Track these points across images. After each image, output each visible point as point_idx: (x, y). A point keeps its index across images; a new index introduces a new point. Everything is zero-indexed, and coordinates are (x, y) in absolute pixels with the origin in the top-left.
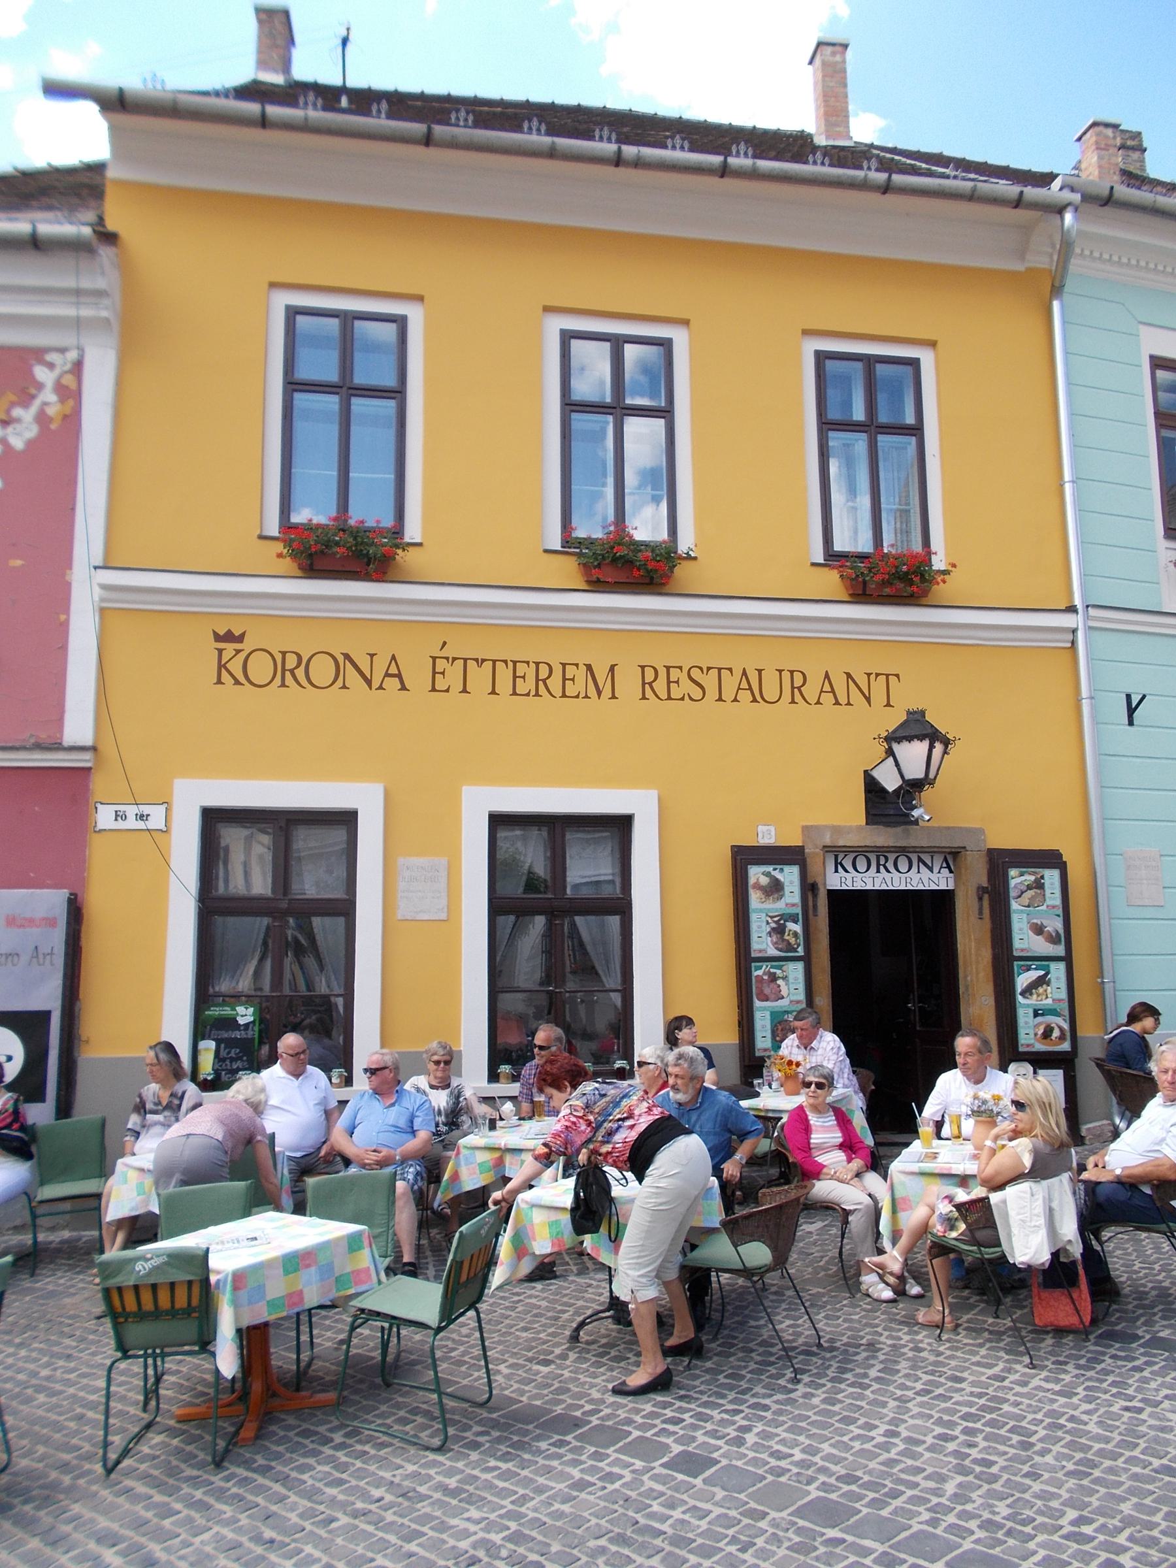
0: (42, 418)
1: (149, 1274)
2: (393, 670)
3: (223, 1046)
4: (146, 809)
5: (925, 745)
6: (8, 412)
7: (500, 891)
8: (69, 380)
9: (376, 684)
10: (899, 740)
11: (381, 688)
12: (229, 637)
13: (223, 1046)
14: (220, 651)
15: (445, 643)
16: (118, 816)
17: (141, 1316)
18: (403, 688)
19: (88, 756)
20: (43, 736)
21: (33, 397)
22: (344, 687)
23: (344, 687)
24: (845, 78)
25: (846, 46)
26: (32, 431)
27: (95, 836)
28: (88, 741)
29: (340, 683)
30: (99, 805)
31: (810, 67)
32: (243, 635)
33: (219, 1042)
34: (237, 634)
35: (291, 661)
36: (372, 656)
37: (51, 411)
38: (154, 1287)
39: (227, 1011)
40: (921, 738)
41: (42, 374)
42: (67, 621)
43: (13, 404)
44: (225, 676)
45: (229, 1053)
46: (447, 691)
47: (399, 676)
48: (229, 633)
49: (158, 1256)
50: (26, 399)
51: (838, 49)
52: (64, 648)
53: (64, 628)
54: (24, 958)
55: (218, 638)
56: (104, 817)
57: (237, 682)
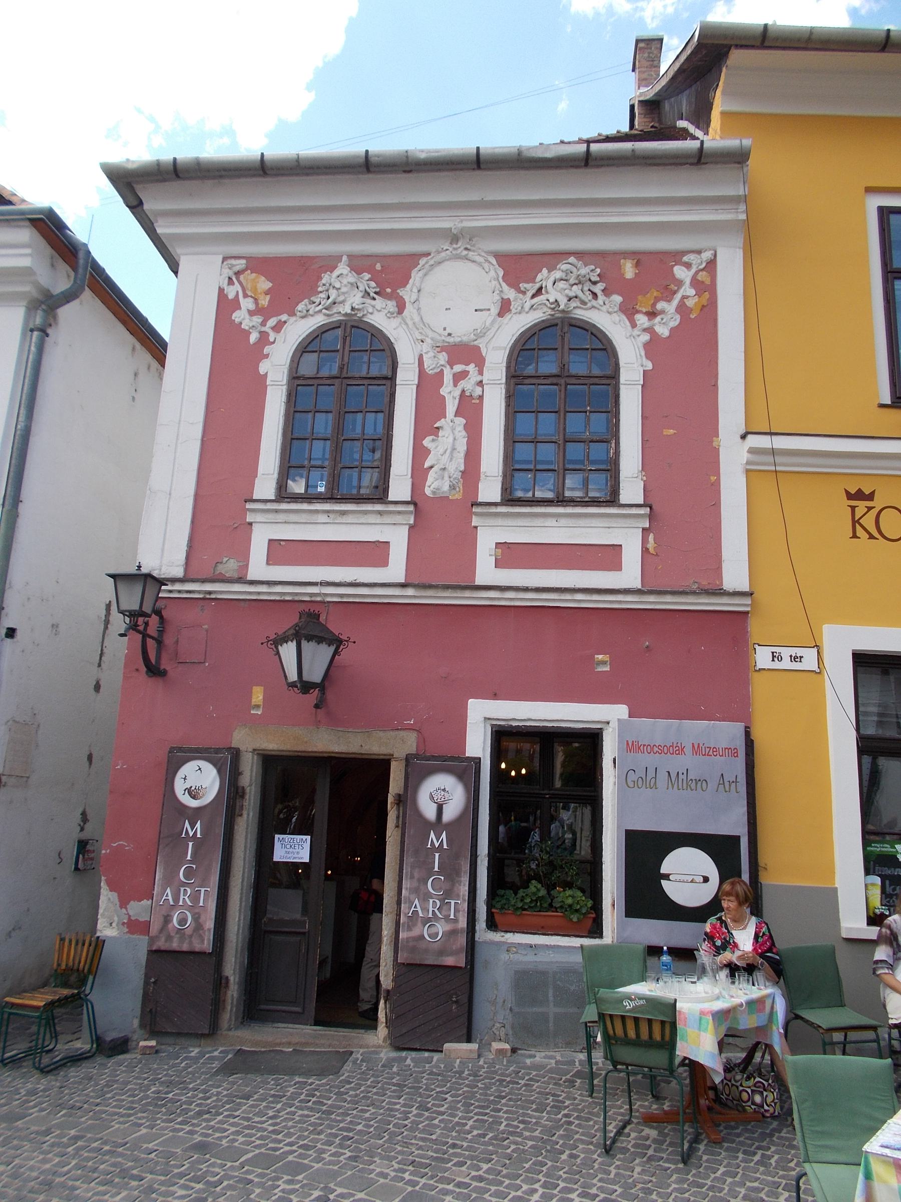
0: (682, 308)
1: (633, 1010)
3: (887, 882)
4: (799, 652)
6: (654, 305)
7: (862, 732)
12: (859, 495)
13: (887, 882)
14: (853, 508)
17: (627, 1042)
19: (748, 601)
20: (704, 583)
21: (675, 292)
26: (675, 321)
27: (756, 675)
28: (745, 587)
30: (756, 647)
32: (873, 493)
33: (883, 878)
37: (690, 303)
38: (636, 1019)
39: (887, 849)
41: (679, 272)
42: (718, 481)
43: (657, 300)
44: (860, 531)
45: (894, 890)
48: (860, 491)
49: (640, 999)
50: (668, 295)
52: (717, 505)
54: (712, 785)
55: (850, 496)
56: (762, 658)
57: (871, 537)
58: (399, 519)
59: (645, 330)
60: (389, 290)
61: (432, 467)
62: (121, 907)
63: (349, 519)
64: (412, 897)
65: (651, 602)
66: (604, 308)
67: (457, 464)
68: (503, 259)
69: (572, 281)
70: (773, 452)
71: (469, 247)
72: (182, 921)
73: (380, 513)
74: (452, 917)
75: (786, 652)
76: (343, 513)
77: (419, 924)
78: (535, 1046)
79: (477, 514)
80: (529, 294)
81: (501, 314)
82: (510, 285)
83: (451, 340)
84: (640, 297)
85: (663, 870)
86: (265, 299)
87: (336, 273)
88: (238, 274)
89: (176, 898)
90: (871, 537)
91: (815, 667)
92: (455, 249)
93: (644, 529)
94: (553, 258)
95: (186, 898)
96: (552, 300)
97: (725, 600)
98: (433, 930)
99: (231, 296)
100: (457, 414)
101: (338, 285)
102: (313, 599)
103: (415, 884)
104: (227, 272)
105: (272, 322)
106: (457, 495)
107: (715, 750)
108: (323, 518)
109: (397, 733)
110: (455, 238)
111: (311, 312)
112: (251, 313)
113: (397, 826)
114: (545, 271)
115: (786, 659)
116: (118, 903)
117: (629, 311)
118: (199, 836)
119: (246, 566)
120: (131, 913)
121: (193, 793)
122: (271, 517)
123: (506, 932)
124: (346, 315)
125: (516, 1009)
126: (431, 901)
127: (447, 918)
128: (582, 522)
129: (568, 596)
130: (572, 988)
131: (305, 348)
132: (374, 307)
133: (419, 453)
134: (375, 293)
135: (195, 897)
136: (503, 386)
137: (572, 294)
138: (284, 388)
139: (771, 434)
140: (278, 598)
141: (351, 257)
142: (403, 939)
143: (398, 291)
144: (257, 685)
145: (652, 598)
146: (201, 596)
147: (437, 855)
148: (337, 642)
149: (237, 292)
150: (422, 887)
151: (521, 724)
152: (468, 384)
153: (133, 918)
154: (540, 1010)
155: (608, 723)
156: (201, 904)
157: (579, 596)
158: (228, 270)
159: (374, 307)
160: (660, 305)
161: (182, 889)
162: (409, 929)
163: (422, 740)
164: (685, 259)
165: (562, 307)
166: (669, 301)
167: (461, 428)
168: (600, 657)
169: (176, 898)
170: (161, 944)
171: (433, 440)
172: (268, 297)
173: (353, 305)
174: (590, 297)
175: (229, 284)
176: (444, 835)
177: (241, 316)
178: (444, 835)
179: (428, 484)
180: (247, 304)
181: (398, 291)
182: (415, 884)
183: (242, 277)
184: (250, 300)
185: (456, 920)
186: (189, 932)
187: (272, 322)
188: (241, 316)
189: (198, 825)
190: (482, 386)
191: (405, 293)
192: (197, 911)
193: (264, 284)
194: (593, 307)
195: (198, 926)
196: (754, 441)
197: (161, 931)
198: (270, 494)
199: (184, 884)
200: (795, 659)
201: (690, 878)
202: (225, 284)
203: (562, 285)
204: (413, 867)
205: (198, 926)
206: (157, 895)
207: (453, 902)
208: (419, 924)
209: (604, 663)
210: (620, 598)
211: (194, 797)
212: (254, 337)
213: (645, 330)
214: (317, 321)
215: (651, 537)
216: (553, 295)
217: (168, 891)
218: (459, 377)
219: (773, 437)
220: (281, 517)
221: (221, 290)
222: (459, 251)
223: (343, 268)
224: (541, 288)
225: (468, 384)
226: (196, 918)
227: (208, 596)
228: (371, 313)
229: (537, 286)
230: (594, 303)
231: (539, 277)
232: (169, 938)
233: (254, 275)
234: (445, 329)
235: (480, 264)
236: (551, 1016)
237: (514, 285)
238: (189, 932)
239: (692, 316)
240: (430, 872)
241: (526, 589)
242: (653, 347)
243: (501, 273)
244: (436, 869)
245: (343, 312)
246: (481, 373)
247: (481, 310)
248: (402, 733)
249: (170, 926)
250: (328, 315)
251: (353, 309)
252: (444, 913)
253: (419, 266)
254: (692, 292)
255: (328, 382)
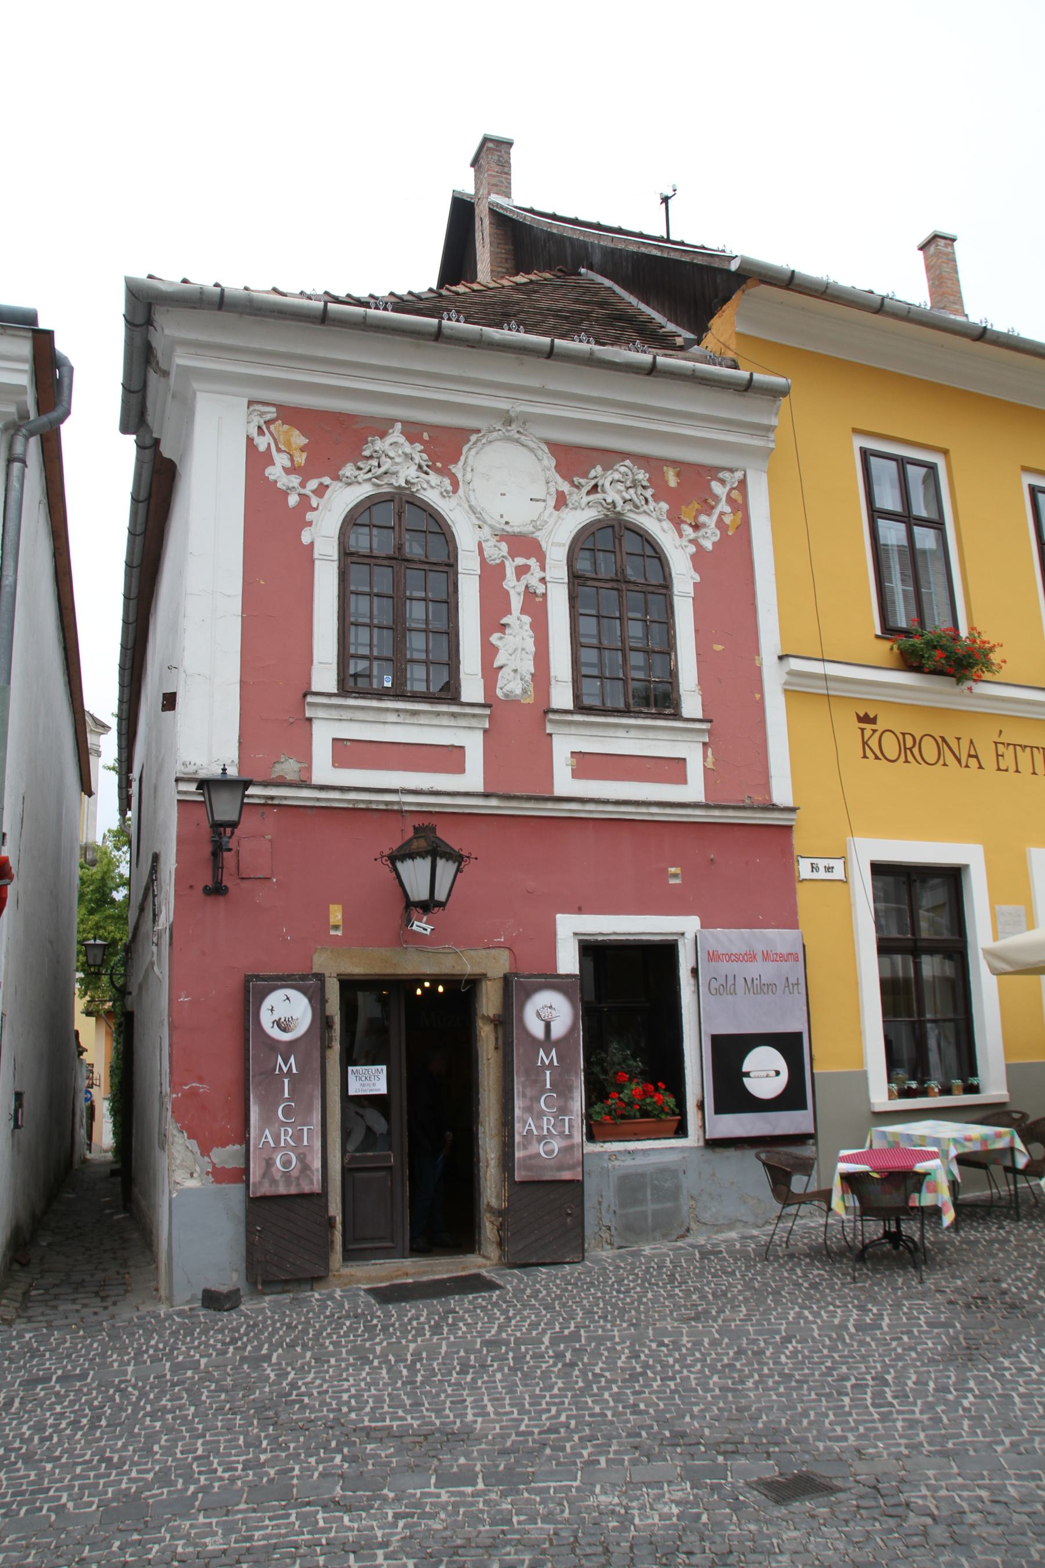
0: (720, 524)
2: (973, 752)
5: (427, 863)
6: (696, 518)
8: (735, 494)
9: (964, 763)
10: (403, 858)
11: (967, 766)
12: (865, 719)
14: (862, 730)
15: (1001, 732)
16: (814, 868)
18: (981, 767)
21: (713, 508)
22: (945, 765)
23: (945, 765)
24: (956, 266)
25: (953, 240)
29: (941, 762)
30: (800, 859)
31: (921, 253)
32: (875, 717)
34: (872, 716)
35: (909, 743)
36: (958, 739)
37: (727, 520)
40: (422, 855)
41: (716, 487)
43: (699, 512)
44: (869, 753)
46: (1006, 770)
47: (976, 757)
48: (866, 715)
50: (709, 509)
51: (949, 242)
53: (761, 705)
56: (804, 869)
57: (877, 758)
58: (474, 723)
59: (690, 541)
60: (439, 465)
61: (501, 667)
62: (203, 1155)
63: (423, 720)
64: (526, 1115)
65: (717, 816)
66: (654, 514)
67: (528, 666)
68: (554, 448)
69: (629, 484)
70: (826, 677)
71: (521, 430)
72: (287, 1163)
73: (454, 715)
74: (567, 1132)
75: (822, 863)
76: (414, 713)
77: (535, 1142)
78: (636, 1242)
79: (552, 721)
80: (585, 490)
81: (557, 508)
82: (564, 477)
83: (507, 528)
84: (683, 507)
85: (745, 1069)
86: (300, 456)
87: (389, 440)
88: (268, 423)
89: (277, 1139)
90: (877, 758)
91: (842, 877)
92: (508, 431)
93: (704, 744)
94: (609, 457)
95: (288, 1138)
96: (609, 500)
97: (776, 815)
98: (549, 1147)
99: (262, 448)
100: (523, 611)
101: (392, 454)
102: (389, 807)
103: (528, 1103)
104: (257, 420)
105: (313, 484)
106: (529, 700)
107: (781, 956)
108: (392, 718)
109: (488, 951)
110: (509, 421)
111: (360, 479)
112: (288, 471)
113: (496, 1048)
114: (599, 468)
115: (822, 869)
116: (199, 1152)
117: (676, 521)
118: (294, 1071)
119: (309, 769)
120: (215, 1160)
121: (283, 1026)
122: (334, 714)
123: (604, 1142)
124: (400, 487)
125: (618, 1212)
126: (545, 1119)
127: (562, 1134)
128: (651, 734)
129: (643, 810)
130: (666, 1185)
131: (352, 521)
132: (428, 482)
133: (489, 652)
134: (428, 466)
135: (298, 1137)
136: (566, 586)
137: (628, 497)
138: (336, 564)
139: (823, 660)
140: (351, 806)
141: (405, 423)
142: (519, 1159)
143: (451, 467)
144: (335, 903)
145: (716, 813)
146: (262, 801)
147: (548, 1073)
148: (457, 858)
149: (269, 444)
150: (535, 1106)
151: (605, 938)
152: (532, 579)
153: (218, 1166)
154: (638, 1209)
155: (683, 934)
156: (305, 1143)
157: (654, 810)
158: (258, 418)
159: (428, 482)
160: (703, 518)
161: (282, 1129)
162: (525, 1147)
163: (514, 958)
164: (721, 475)
165: (618, 509)
166: (709, 515)
167: (527, 627)
168: (672, 870)
169: (277, 1139)
170: (266, 1190)
171: (501, 638)
172: (304, 455)
173: (409, 478)
174: (643, 502)
175: (259, 434)
176: (554, 1053)
177: (275, 473)
178: (554, 1053)
179: (499, 685)
180: (281, 460)
181: (451, 467)
182: (528, 1103)
183: (272, 427)
184: (285, 456)
185: (570, 1136)
186: (295, 1174)
187: (313, 484)
188: (275, 473)
189: (292, 1060)
190: (545, 584)
191: (457, 469)
192: (301, 1151)
193: (299, 440)
194: (645, 512)
195: (305, 1167)
196: (795, 664)
197: (264, 1176)
198: (332, 687)
199: (284, 1124)
200: (829, 869)
201: (765, 1074)
202: (254, 432)
203: (620, 487)
204: (524, 1087)
205: (305, 1167)
206: (255, 1139)
207: (567, 1119)
208: (535, 1142)
209: (675, 876)
210: (689, 811)
211: (285, 1030)
212: (293, 500)
213: (690, 541)
214: (365, 491)
215: (710, 751)
216: (612, 495)
217: (267, 1132)
218: (521, 571)
219: (826, 664)
220: (346, 715)
221: (250, 440)
222: (512, 433)
223: (396, 435)
224: (596, 486)
225: (532, 579)
226: (302, 1159)
227: (270, 802)
228: (425, 489)
229: (593, 482)
230: (645, 508)
231: (592, 474)
232: (274, 1182)
233: (286, 427)
234: (502, 516)
235: (531, 450)
236: (650, 1214)
237: (567, 477)
238: (295, 1174)
239: (730, 533)
240: (543, 1091)
241: (606, 802)
242: (699, 560)
243: (554, 463)
244: (548, 1086)
245: (396, 485)
246: (543, 568)
247: (537, 500)
248: (493, 952)
249: (273, 1169)
250: (378, 486)
251: (407, 482)
252: (559, 1129)
253: (471, 443)
254: (728, 509)
255: (385, 562)
